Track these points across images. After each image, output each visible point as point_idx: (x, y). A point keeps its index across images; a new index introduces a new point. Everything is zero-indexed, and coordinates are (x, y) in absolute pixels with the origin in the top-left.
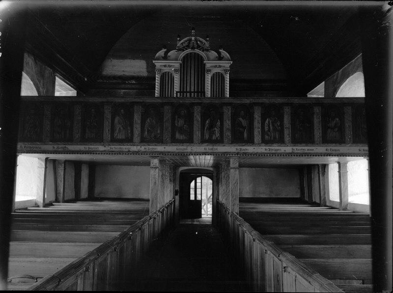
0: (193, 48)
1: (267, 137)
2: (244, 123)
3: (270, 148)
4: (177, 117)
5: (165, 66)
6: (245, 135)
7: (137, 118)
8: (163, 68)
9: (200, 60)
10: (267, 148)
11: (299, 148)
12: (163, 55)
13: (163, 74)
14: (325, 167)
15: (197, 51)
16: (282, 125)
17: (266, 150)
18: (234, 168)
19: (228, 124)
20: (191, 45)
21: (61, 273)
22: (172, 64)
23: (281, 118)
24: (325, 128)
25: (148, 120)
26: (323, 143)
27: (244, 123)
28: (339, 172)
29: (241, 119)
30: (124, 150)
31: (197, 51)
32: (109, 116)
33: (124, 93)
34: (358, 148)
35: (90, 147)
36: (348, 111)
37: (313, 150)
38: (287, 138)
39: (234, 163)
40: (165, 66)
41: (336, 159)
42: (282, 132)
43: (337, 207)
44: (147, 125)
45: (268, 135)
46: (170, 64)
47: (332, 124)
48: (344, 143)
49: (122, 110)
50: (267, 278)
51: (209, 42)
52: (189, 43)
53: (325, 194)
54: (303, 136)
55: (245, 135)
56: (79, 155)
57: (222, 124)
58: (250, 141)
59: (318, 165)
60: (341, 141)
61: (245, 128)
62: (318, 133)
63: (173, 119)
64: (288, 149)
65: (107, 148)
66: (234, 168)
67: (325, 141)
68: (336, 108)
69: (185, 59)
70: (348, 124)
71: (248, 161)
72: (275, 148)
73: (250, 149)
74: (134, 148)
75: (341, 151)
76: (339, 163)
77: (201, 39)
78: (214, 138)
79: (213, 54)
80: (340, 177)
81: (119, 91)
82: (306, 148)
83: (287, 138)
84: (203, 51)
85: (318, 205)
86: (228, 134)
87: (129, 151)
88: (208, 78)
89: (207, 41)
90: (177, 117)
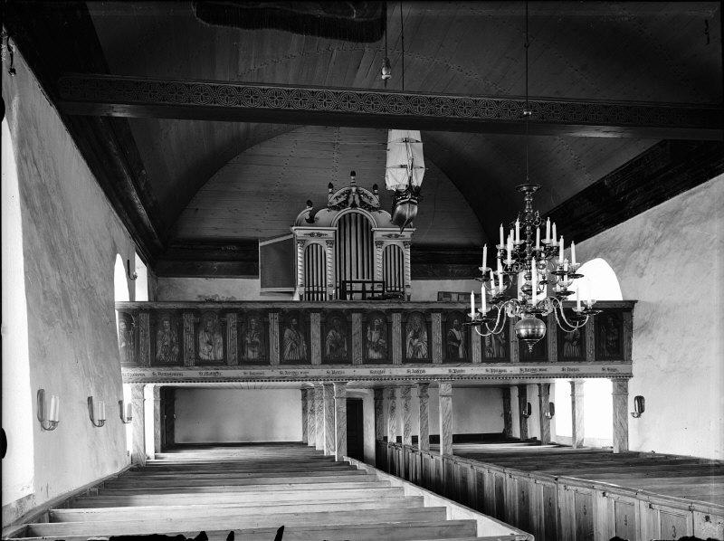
0: (354, 205)
1: (488, 355)
2: (459, 335)
3: (493, 368)
4: (369, 328)
5: (312, 235)
7: (315, 330)
8: (309, 238)
9: (366, 230)
10: (489, 368)
12: (308, 217)
13: (308, 247)
15: (360, 210)
17: (487, 371)
19: (437, 337)
20: (351, 201)
21: (538, 468)
22: (323, 232)
25: (331, 334)
26: (559, 361)
28: (573, 395)
29: (454, 330)
30: (300, 375)
31: (360, 210)
32: (276, 329)
33: (219, 267)
35: (253, 371)
40: (312, 235)
43: (568, 444)
44: (328, 343)
45: (490, 351)
46: (320, 232)
49: (294, 320)
51: (377, 196)
52: (348, 197)
58: (467, 360)
60: (581, 358)
61: (459, 342)
63: (364, 331)
65: (276, 373)
69: (343, 223)
71: (461, 382)
73: (468, 370)
75: (581, 371)
77: (366, 191)
78: (420, 356)
79: (385, 216)
80: (573, 403)
81: (210, 263)
83: (514, 355)
84: (370, 210)
85: (539, 443)
86: (438, 351)
87: (307, 377)
88: (378, 253)
89: (375, 194)
90: (369, 328)
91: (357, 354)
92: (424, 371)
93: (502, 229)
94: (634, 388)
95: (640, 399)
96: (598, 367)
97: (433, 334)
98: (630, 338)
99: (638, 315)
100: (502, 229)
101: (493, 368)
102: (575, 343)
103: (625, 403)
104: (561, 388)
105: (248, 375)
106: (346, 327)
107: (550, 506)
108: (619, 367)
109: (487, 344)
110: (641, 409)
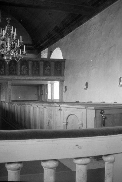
1: (22, 73)
2: (14, 67)
6: (14, 72)
7: (30, 66)
10: (12, 77)
11: (34, 77)
14: (47, 85)
16: (28, 68)
18: (10, 85)
23: (27, 65)
24: (44, 70)
27: (14, 67)
34: (56, 78)
36: (53, 64)
37: (39, 78)
38: (30, 73)
39: (9, 83)
41: (50, 81)
42: (28, 71)
47: (47, 68)
48: (39, 75)
50: (22, 112)
53: (46, 97)
54: (36, 72)
55: (14, 72)
56: (18, 78)
57: (5, 67)
59: (44, 84)
60: (50, 75)
62: (41, 72)
64: (30, 78)
66: (10, 85)
67: (44, 75)
68: (48, 62)
70: (52, 69)
72: (25, 77)
73: (16, 77)
74: (28, 78)
76: (51, 83)
80: (51, 89)
82: (37, 77)
83: (30, 73)
86: (7, 71)
91: (19, 73)
92: (3, 78)
93: (1, 29)
94: (65, 84)
95: (66, 87)
96: (55, 78)
97: (6, 67)
98: (64, 70)
99: (66, 62)
100: (1, 29)
101: (58, 78)
102: (48, 71)
103: (63, 89)
104: (49, 83)
105: (12, 78)
106: (38, 66)
107: (35, 113)
108: (61, 78)
109: (22, 70)
110: (66, 90)
